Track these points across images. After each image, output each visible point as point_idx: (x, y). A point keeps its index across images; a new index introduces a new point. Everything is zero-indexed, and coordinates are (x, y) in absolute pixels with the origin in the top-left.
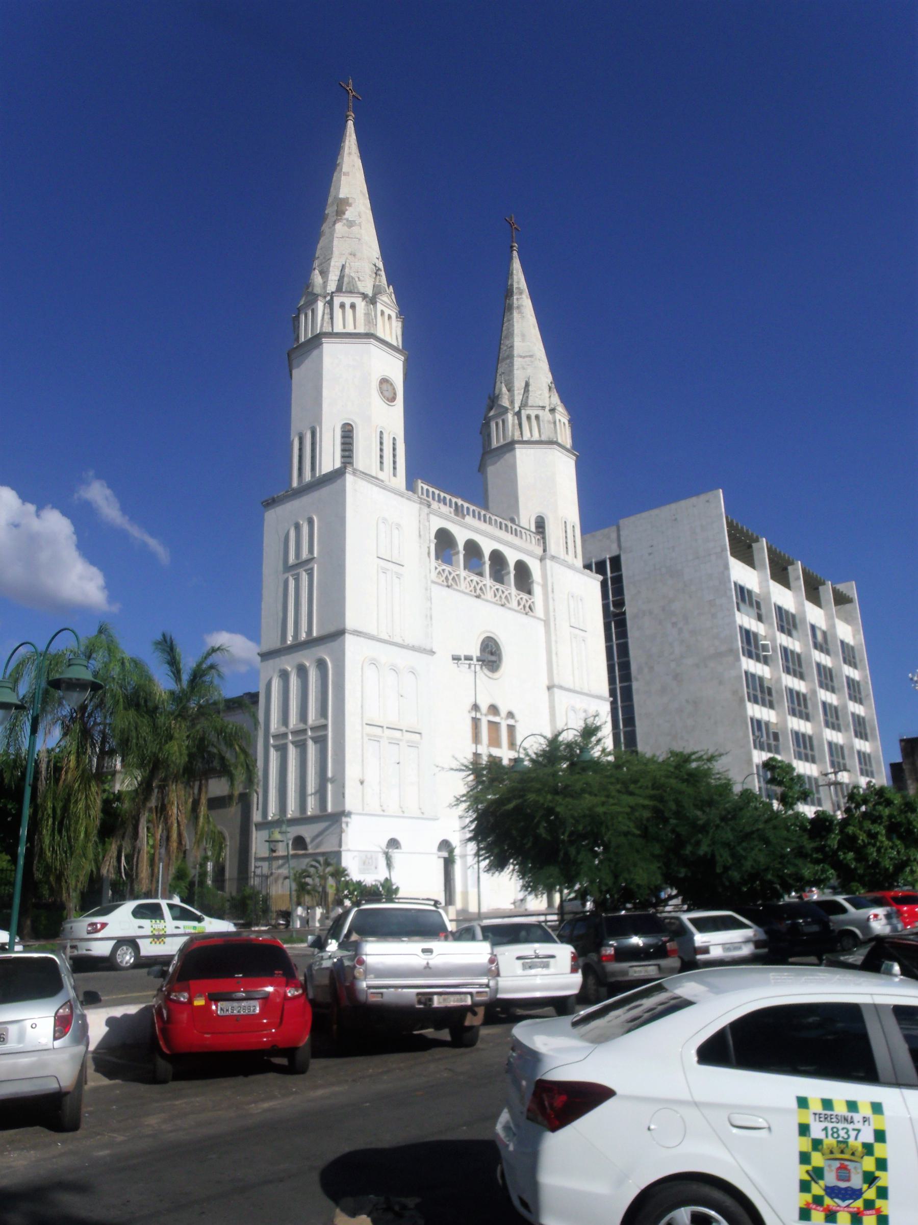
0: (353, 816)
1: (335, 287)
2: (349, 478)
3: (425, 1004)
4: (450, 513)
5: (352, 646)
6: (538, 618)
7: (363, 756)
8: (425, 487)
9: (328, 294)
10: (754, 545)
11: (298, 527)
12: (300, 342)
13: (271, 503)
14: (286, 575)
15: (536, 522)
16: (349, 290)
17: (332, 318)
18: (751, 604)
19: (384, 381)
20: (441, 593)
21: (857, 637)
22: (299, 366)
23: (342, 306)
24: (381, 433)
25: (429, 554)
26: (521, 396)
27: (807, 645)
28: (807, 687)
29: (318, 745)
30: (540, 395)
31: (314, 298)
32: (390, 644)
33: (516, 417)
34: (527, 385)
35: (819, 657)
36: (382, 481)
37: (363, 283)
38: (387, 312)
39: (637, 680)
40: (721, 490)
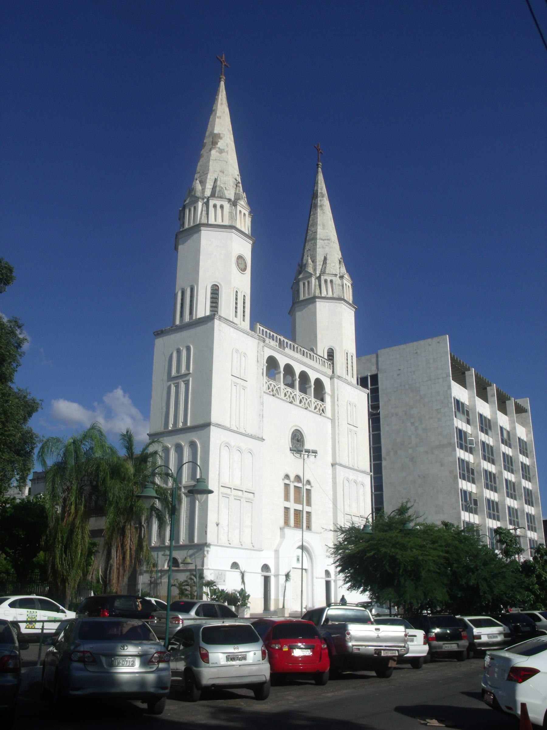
0: (211, 547)
1: (210, 193)
2: (216, 322)
3: (378, 654)
4: (276, 346)
5: (214, 432)
6: (328, 418)
7: (218, 508)
8: (262, 328)
9: (205, 197)
10: (466, 372)
11: (179, 352)
12: (185, 228)
13: (160, 333)
14: (169, 383)
15: (328, 352)
16: (219, 196)
17: (208, 214)
18: (463, 413)
19: (240, 258)
20: (268, 399)
21: (529, 436)
22: (183, 243)
23: (215, 206)
24: (237, 292)
25: (263, 373)
26: (321, 266)
27: (497, 441)
28: (496, 469)
29: (189, 498)
30: (334, 266)
31: (196, 200)
32: (348, 468)
33: (317, 281)
34: (325, 259)
35: (504, 449)
36: (237, 324)
37: (228, 191)
38: (243, 211)
39: (385, 460)
40: (448, 336)
